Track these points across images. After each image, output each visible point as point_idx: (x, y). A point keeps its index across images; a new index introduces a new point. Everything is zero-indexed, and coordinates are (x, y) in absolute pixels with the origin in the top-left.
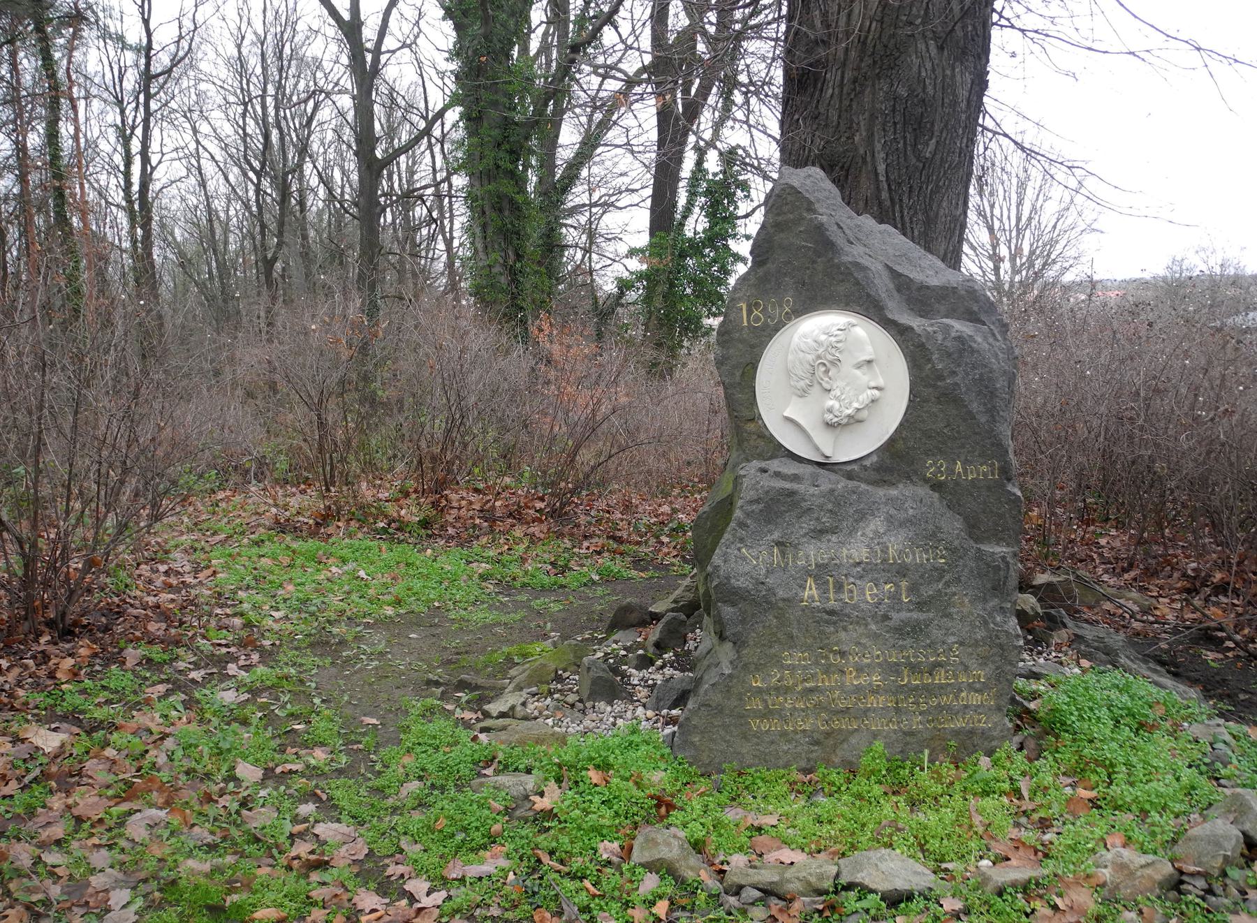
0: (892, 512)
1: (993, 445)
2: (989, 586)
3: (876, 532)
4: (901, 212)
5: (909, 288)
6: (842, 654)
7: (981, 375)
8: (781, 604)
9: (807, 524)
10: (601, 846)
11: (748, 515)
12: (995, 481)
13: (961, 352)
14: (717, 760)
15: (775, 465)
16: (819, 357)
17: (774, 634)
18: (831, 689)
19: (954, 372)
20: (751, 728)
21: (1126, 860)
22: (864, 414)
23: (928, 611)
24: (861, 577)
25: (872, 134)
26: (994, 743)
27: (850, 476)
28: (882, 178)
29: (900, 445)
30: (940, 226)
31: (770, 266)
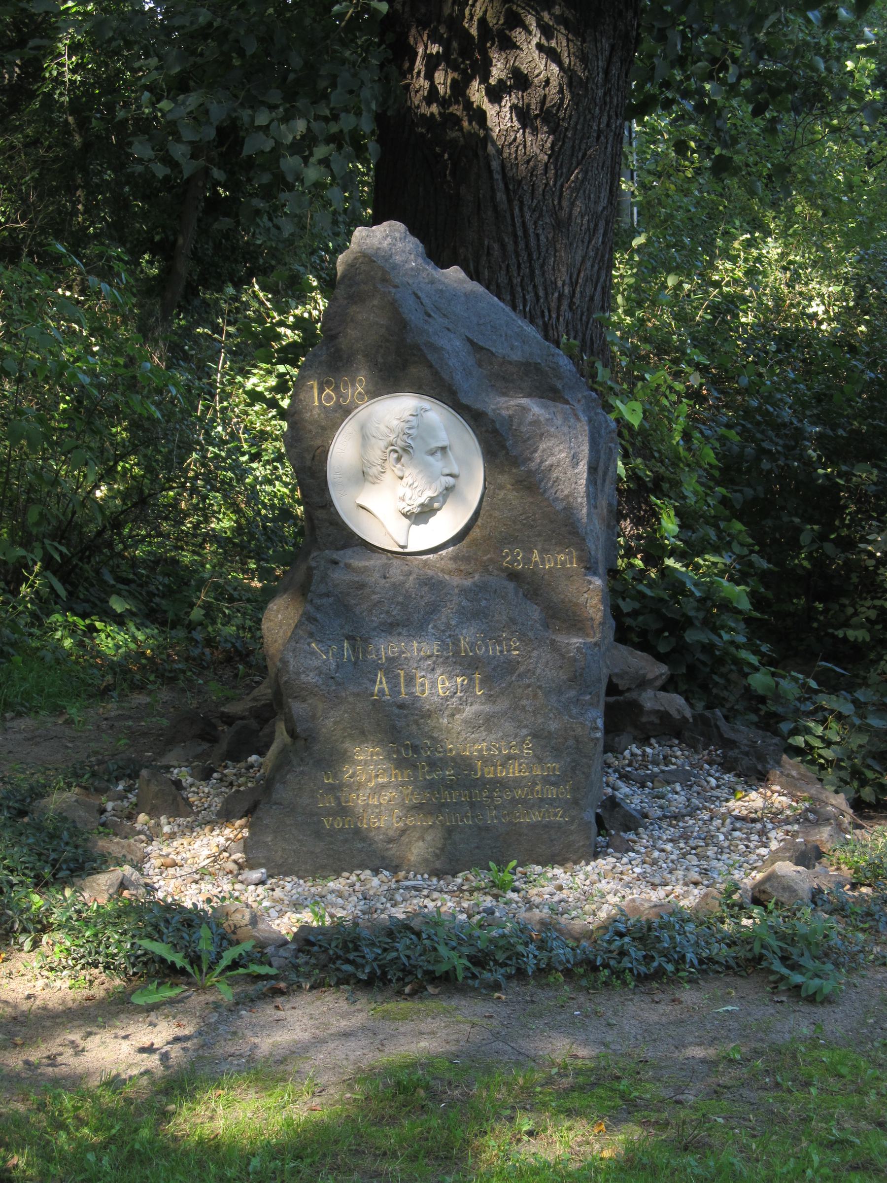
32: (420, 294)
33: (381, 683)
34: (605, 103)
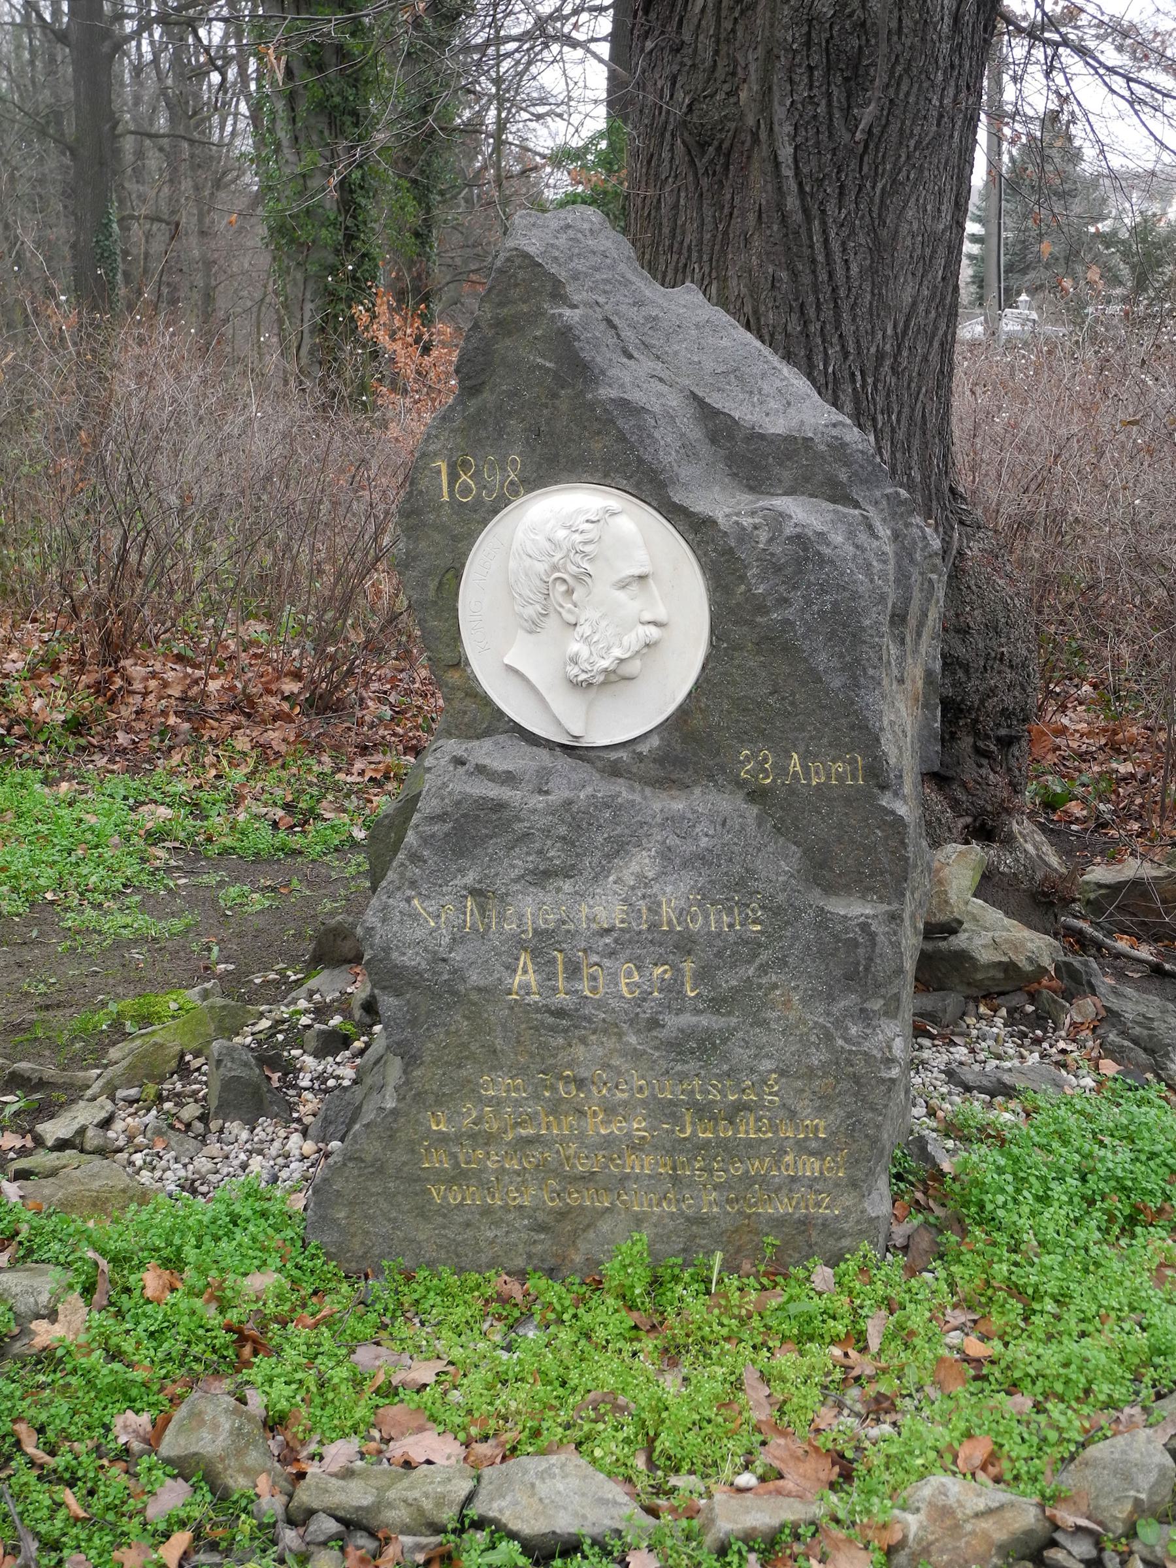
0: (673, 840)
1: (852, 727)
2: (838, 973)
3: (640, 877)
4: (824, 232)
5: (731, 437)
6: (580, 1083)
7: (835, 604)
8: (474, 997)
9: (521, 861)
10: (119, 1422)
11: (426, 840)
12: (858, 789)
13: (800, 563)
14: (376, 1251)
15: (484, 752)
16: (555, 568)
17: (465, 1046)
18: (563, 1141)
19: (786, 600)
20: (431, 1201)
21: (951, 1501)
22: (634, 667)
23: (730, 1013)
24: (612, 954)
25: (770, 88)
26: (846, 1242)
27: (614, 771)
28: (788, 172)
29: (697, 721)
30: (902, 255)
31: (488, 397)
32: (616, 320)
33: (525, 972)
34: (952, 66)
